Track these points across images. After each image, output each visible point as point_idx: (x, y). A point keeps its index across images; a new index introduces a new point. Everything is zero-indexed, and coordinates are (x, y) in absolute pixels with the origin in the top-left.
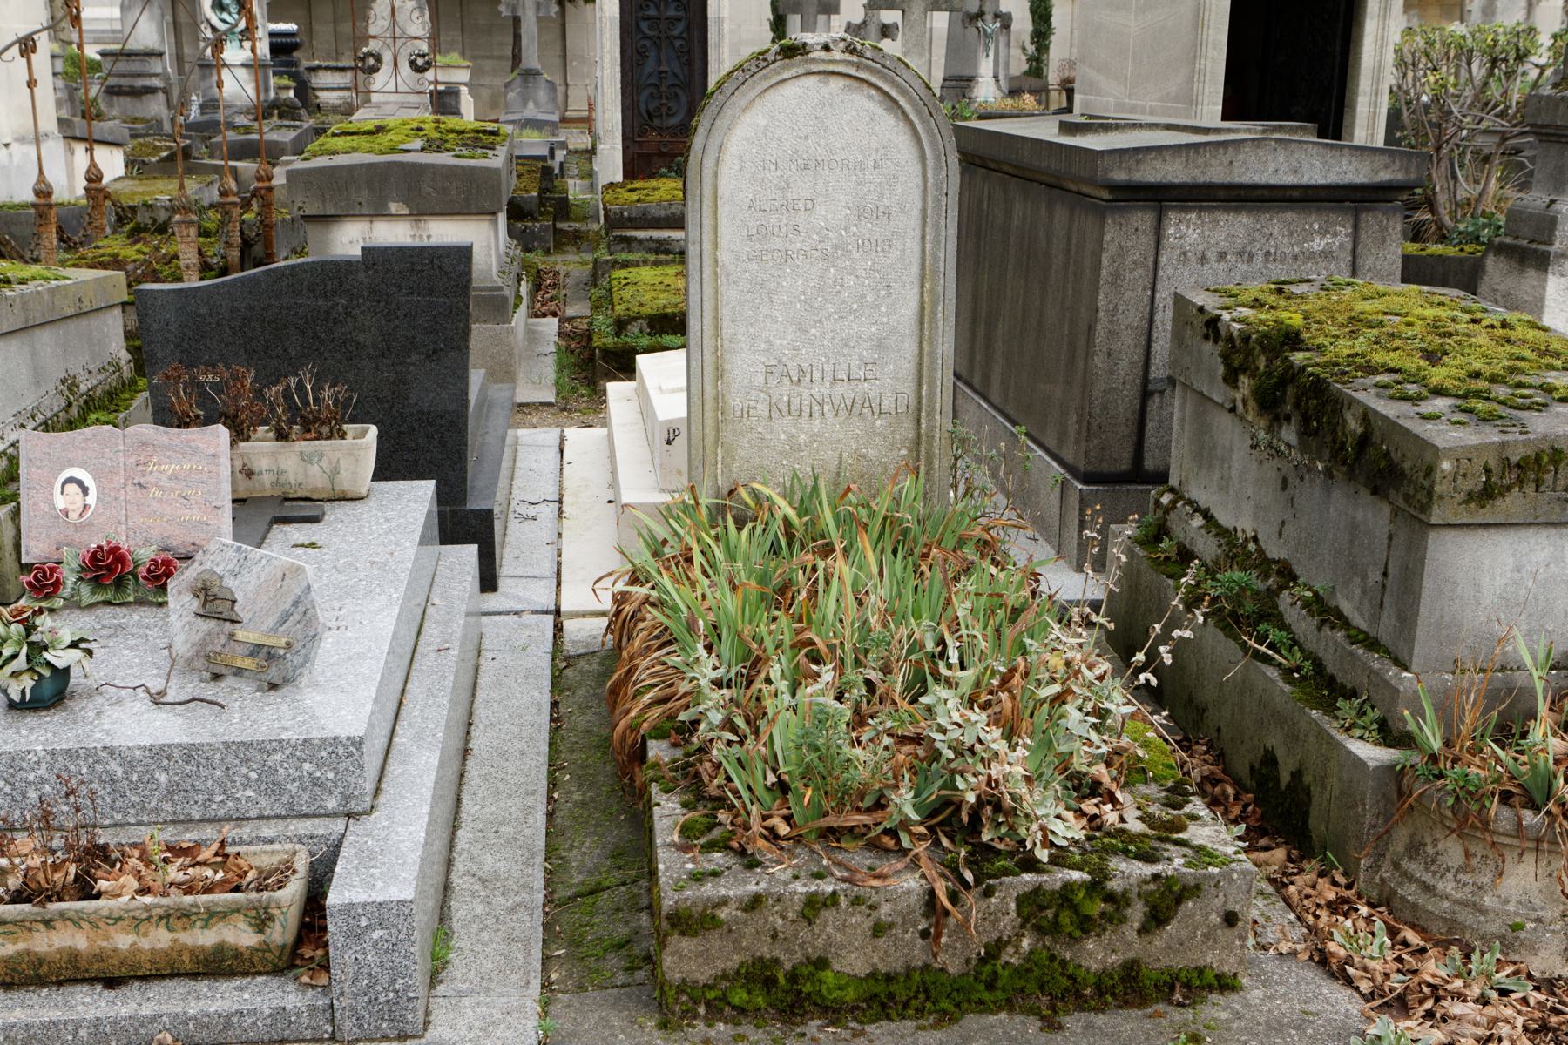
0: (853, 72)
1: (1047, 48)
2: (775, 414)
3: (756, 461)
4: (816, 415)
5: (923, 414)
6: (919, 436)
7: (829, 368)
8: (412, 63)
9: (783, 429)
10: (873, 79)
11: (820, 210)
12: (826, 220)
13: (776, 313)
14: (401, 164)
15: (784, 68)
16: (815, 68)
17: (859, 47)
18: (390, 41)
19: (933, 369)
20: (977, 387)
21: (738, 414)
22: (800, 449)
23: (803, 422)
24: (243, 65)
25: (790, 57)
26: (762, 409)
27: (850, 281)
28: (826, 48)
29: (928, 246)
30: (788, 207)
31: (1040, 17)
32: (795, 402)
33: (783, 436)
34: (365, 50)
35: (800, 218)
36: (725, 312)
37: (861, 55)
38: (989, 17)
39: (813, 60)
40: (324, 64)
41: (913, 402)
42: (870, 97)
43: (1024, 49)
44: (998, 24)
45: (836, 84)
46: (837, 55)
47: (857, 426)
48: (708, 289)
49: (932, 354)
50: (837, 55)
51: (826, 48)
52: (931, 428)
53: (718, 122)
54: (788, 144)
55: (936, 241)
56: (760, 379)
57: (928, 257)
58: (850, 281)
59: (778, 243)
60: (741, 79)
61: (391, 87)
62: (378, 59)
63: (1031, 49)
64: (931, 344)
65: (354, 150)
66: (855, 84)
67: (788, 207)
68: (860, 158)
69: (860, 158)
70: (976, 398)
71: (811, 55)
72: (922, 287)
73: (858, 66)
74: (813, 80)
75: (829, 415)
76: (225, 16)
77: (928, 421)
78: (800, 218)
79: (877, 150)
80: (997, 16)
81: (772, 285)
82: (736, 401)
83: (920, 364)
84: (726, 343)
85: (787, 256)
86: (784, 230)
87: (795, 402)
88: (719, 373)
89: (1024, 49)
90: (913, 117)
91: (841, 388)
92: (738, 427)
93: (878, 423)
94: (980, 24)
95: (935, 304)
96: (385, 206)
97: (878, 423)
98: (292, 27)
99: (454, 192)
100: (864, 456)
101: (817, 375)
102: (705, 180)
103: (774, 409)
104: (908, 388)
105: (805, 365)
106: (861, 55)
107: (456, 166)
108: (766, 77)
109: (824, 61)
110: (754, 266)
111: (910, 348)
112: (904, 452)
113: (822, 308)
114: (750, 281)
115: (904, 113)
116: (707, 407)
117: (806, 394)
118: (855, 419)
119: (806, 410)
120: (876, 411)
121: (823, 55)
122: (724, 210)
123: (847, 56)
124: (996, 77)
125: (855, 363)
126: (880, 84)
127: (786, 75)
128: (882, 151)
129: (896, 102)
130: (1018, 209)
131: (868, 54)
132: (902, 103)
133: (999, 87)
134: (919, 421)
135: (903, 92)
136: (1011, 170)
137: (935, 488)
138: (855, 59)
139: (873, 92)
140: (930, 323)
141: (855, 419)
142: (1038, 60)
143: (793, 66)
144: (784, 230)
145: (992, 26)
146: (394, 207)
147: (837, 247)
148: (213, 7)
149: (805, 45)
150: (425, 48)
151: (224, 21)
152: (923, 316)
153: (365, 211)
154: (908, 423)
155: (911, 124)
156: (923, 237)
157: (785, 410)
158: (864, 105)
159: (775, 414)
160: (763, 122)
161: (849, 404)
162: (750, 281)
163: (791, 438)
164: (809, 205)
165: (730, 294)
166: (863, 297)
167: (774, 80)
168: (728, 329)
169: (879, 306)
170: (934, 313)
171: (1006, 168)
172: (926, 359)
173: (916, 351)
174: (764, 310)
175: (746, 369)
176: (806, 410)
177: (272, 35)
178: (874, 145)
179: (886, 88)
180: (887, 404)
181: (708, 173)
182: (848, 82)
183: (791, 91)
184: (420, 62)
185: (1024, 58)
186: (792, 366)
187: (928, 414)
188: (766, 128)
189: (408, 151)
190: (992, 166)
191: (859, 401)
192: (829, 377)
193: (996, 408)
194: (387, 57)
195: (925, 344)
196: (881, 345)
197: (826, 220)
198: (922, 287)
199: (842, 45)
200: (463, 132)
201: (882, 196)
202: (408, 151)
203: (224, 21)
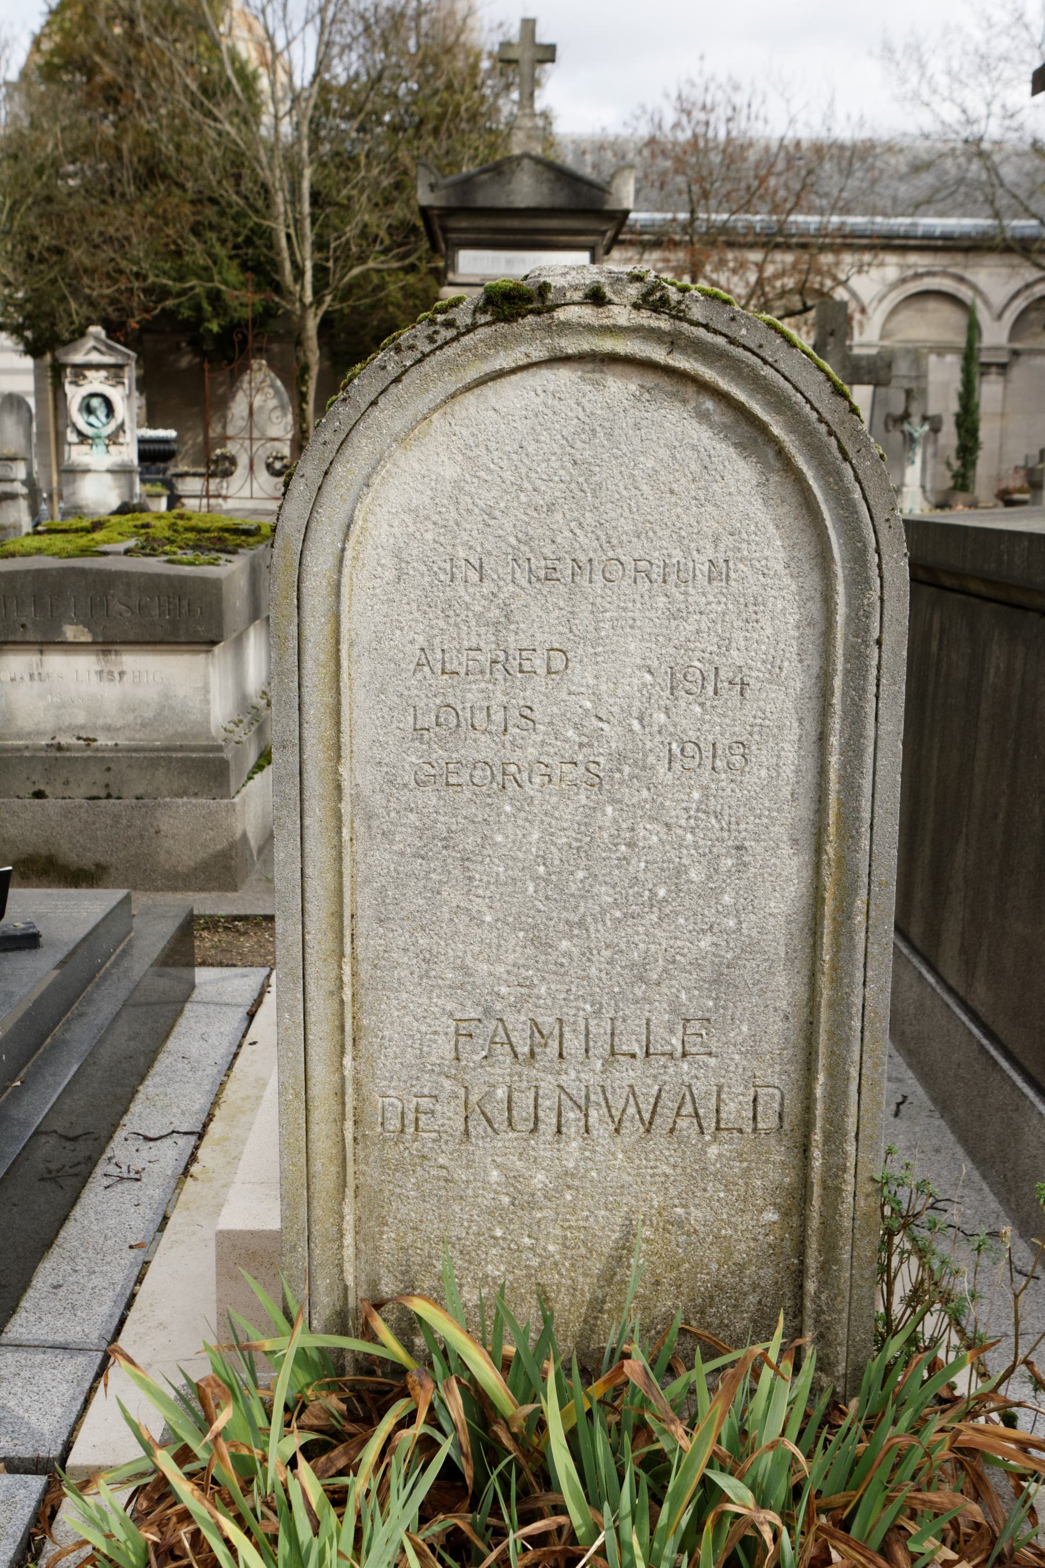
0: (658, 354)
1: (973, 464)
2: (478, 1127)
3: (433, 1228)
4: (571, 1131)
5: (817, 1137)
6: (805, 1183)
7: (600, 1029)
8: (269, 466)
9: (495, 1164)
10: (709, 374)
11: (582, 675)
12: (597, 698)
13: (478, 905)
14: (83, 572)
15: (497, 344)
16: (571, 345)
17: (674, 295)
18: (247, 443)
19: (839, 1039)
20: (918, 943)
21: (394, 1124)
22: (532, 1205)
23: (543, 1145)
24: (109, 471)
25: (508, 319)
26: (450, 1116)
27: (651, 834)
28: (596, 297)
29: (834, 760)
30: (508, 665)
31: (967, 431)
32: (524, 1102)
33: (495, 1175)
34: (218, 451)
35: (534, 692)
36: (362, 901)
37: (679, 315)
38: (916, 419)
39: (566, 327)
40: (192, 470)
41: (793, 1108)
42: (703, 416)
43: (949, 465)
44: (926, 428)
45: (619, 387)
46: (621, 315)
47: (664, 1158)
48: (318, 851)
49: (840, 1006)
50: (621, 315)
51: (596, 297)
52: (834, 1172)
53: (339, 469)
54: (508, 523)
55: (853, 749)
56: (444, 1048)
57: (834, 786)
58: (651, 834)
59: (484, 747)
60: (393, 369)
61: (246, 492)
62: (233, 461)
63: (956, 464)
64: (837, 982)
65: (39, 551)
66: (665, 383)
67: (508, 665)
68: (677, 555)
69: (677, 555)
70: (916, 961)
71: (561, 315)
72: (818, 850)
73: (673, 342)
74: (564, 376)
75: (601, 1131)
76: (92, 419)
77: (827, 1154)
78: (534, 692)
79: (716, 540)
80: (925, 419)
81: (470, 842)
82: (388, 1097)
83: (811, 1026)
84: (365, 969)
85: (504, 777)
86: (498, 717)
87: (524, 1102)
88: (348, 1036)
89: (949, 465)
90: (801, 462)
91: (626, 1074)
92: (392, 1153)
93: (713, 1151)
94: (906, 427)
95: (846, 892)
96: (59, 631)
97: (713, 1151)
98: (172, 433)
99: (156, 612)
100: (680, 1223)
101: (574, 1044)
102: (308, 603)
103: (477, 1115)
104: (776, 1080)
105: (547, 1021)
106: (679, 315)
107: (168, 577)
108: (453, 366)
109: (590, 329)
110: (429, 798)
111: (784, 988)
112: (771, 1216)
113: (586, 894)
114: (420, 832)
115: (781, 452)
116: (316, 1115)
117: (548, 1084)
118: (659, 1141)
119: (549, 1120)
120: (710, 1124)
121: (587, 314)
122: (357, 671)
123: (646, 318)
124: (923, 487)
125: (661, 1018)
126: (724, 384)
127: (503, 360)
128: (727, 541)
129: (762, 428)
130: (997, 656)
131: (697, 313)
132: (776, 430)
133: (926, 499)
134: (805, 1150)
135: (779, 403)
136: (983, 590)
137: (842, 1304)
138: (664, 323)
139: (709, 405)
140: (837, 934)
141: (659, 1141)
142: (964, 476)
143: (519, 339)
144: (498, 717)
145: (920, 430)
146: (70, 632)
147: (622, 757)
148: (80, 410)
149: (544, 289)
150: (286, 451)
151: (91, 425)
152: (818, 920)
153: (30, 637)
154: (779, 1153)
155: (799, 478)
156: (822, 738)
157: (500, 1119)
158: (681, 431)
159: (478, 1127)
160: (450, 472)
161: (647, 1109)
162: (420, 832)
163: (512, 1178)
164: (558, 663)
165: (372, 860)
166: (680, 871)
167: (473, 373)
168: (369, 941)
169: (717, 893)
170: (844, 913)
171: (973, 586)
172: (824, 1014)
173: (803, 994)
174: (451, 895)
175: (410, 1027)
176: (549, 1120)
177: (141, 441)
178: (710, 527)
179: (740, 395)
180: (735, 1109)
181: (316, 586)
182: (651, 379)
183: (515, 396)
184: (278, 465)
185: (949, 474)
186: (518, 1023)
187: (828, 1138)
188: (458, 485)
189: (105, 554)
190: (947, 581)
191: (669, 1104)
192: (600, 1048)
193: (950, 990)
194: (243, 461)
195: (824, 982)
196: (719, 979)
197: (597, 698)
198: (818, 850)
199: (634, 291)
200: (207, 531)
201: (726, 644)
202: (105, 554)
203: (91, 425)
